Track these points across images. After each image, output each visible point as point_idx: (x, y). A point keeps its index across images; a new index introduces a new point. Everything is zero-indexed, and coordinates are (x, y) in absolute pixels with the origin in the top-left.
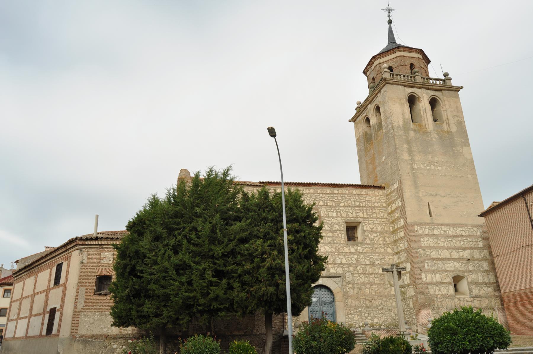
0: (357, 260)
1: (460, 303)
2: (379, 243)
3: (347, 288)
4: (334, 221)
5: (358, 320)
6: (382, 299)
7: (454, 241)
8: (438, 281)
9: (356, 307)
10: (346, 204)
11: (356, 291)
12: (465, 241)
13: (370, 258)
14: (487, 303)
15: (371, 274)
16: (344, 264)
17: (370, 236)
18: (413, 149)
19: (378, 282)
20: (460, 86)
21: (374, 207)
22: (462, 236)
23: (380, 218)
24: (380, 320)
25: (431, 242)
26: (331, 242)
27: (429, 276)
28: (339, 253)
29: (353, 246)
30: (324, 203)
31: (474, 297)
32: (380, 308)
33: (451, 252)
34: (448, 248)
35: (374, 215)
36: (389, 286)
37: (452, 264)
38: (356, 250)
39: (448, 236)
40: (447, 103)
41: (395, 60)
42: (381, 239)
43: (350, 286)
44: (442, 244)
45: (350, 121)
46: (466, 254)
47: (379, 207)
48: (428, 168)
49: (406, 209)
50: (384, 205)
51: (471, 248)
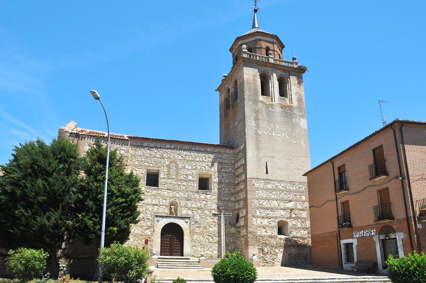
7: (283, 194)
10: (201, 160)
21: (224, 163)
25: (264, 194)
27: (259, 221)
35: (223, 170)
39: (279, 190)
42: (227, 189)
45: (216, 90)
48: (270, 134)
49: (247, 166)
50: (233, 162)
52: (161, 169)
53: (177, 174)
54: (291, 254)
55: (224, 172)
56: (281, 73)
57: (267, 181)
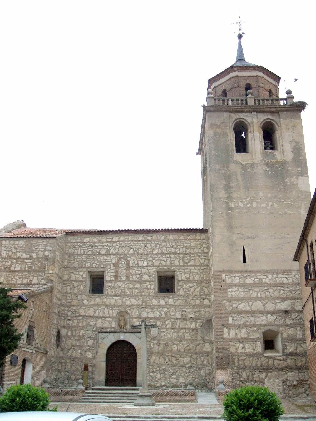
1: (268, 362)
2: (194, 294)
3: (152, 344)
4: (144, 270)
5: (160, 379)
6: (191, 357)
7: (271, 290)
8: (243, 336)
9: (159, 365)
10: (160, 252)
11: (161, 347)
12: (286, 289)
13: (183, 311)
14: (304, 362)
15: (182, 329)
17: (185, 286)
18: (231, 185)
19: (189, 338)
20: (202, 108)
22: (282, 284)
23: (199, 266)
24: (186, 380)
25: (241, 293)
26: (139, 294)
28: (146, 307)
29: (163, 298)
30: (135, 251)
31: (287, 355)
32: (187, 366)
33: (266, 304)
34: (261, 299)
35: (192, 263)
36: (202, 342)
37: (264, 318)
38: (166, 302)
39: (264, 285)
40: (283, 126)
41: (229, 82)
43: (155, 342)
44: (254, 295)
46: (284, 306)
47: (199, 253)
48: (249, 205)
52: (107, 269)
53: (128, 274)
54: (287, 380)
55: (193, 266)
56: (266, 117)
57: (245, 274)
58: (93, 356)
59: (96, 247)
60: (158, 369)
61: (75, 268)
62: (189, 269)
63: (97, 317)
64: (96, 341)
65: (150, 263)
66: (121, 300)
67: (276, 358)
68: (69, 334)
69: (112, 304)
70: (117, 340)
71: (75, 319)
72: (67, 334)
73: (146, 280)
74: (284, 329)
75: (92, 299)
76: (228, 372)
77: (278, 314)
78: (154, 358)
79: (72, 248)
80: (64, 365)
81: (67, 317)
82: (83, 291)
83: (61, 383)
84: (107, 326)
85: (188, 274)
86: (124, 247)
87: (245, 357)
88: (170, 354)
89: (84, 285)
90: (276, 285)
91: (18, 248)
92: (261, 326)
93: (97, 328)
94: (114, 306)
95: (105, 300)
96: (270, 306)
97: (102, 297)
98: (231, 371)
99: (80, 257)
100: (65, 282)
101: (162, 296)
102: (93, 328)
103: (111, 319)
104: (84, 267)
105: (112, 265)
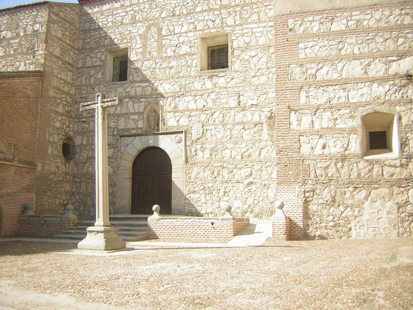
0: (214, 101)
10: (205, 8)
15: (238, 124)
16: (192, 110)
25: (321, 49)
29: (211, 77)
37: (365, 90)
38: (215, 85)
39: (367, 31)
51: (95, 35)
53: (160, 47)
58: (113, 172)
59: (118, 15)
60: (202, 187)
61: (91, 49)
62: (249, 28)
63: (119, 115)
64: (116, 150)
65: (192, 26)
66: (150, 87)
67: (387, 163)
68: (85, 142)
69: (139, 94)
70: (145, 146)
71: (91, 121)
72: (82, 142)
73: (185, 53)
74: (403, 108)
75: (112, 90)
76: (297, 188)
77: (392, 82)
78: (195, 170)
79: (88, 22)
80: (78, 185)
81: (81, 118)
82: (102, 80)
83: (76, 211)
84: (132, 127)
85: (247, 36)
86: (155, 9)
87: (328, 163)
88: (220, 164)
89: (102, 71)
90: (390, 30)
91: (3, 26)
92: (358, 105)
93: (118, 130)
94: (141, 97)
95: (129, 89)
96: (377, 69)
97: (125, 86)
98: (303, 187)
99: (98, 33)
100: (80, 71)
101: (208, 75)
102: (114, 132)
103: (136, 117)
104: (102, 46)
105: (138, 37)
